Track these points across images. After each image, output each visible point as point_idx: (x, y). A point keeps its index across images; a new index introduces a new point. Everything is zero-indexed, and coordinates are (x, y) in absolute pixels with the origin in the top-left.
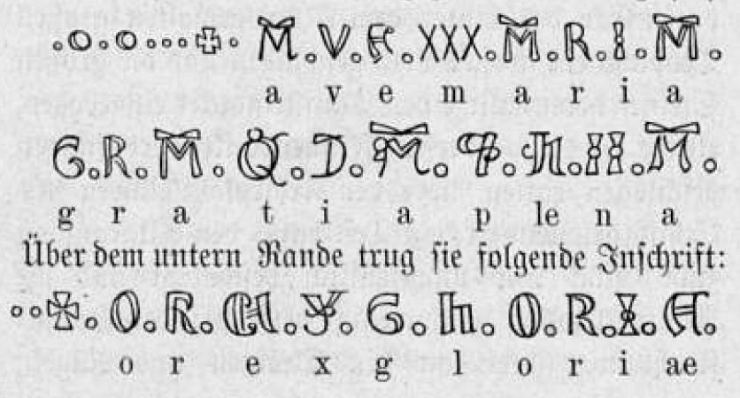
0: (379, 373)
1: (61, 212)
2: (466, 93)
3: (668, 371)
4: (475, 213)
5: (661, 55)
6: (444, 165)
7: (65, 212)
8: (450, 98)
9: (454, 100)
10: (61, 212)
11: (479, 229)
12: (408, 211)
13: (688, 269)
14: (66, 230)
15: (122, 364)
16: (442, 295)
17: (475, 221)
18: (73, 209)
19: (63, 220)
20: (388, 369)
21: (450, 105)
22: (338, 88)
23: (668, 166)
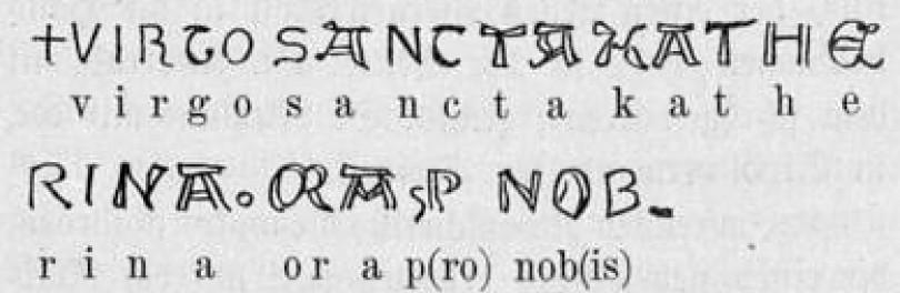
0: (192, 115)
1: (192, 102)
2: (795, 104)
3: (198, 274)
4: (406, 264)
5: (500, 61)
7: (197, 103)
8: (138, 273)
10: (192, 102)
11: (411, 285)
12: (209, 262)
15: (237, 106)
17: (406, 274)
18: (208, 98)
22: (87, 98)
23: (616, 67)
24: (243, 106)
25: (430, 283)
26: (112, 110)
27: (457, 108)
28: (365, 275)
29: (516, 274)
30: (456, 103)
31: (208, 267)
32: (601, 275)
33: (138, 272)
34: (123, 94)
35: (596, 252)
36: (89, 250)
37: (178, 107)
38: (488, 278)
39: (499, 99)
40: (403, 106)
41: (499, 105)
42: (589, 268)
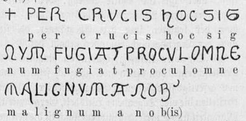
0: (232, 38)
6: (139, 84)
8: (34, 72)
9: (36, 73)
12: (26, 111)
13: (239, 11)
14: (57, 118)
15: (151, 71)
16: (99, 115)
19: (56, 114)
20: (235, 37)
21: (34, 74)
24: (222, 71)
25: (167, 117)
26: (177, 71)
27: (127, 37)
28: (23, 114)
29: (136, 114)
30: (193, 35)
31: (121, 113)
32: (173, 114)
33: (138, 115)
34: (91, 68)
35: (172, 108)
36: (46, 108)
37: (169, 71)
38: (181, 115)
39: (114, 69)
40: (69, 71)
41: (56, 70)
42: (170, 113)
